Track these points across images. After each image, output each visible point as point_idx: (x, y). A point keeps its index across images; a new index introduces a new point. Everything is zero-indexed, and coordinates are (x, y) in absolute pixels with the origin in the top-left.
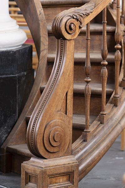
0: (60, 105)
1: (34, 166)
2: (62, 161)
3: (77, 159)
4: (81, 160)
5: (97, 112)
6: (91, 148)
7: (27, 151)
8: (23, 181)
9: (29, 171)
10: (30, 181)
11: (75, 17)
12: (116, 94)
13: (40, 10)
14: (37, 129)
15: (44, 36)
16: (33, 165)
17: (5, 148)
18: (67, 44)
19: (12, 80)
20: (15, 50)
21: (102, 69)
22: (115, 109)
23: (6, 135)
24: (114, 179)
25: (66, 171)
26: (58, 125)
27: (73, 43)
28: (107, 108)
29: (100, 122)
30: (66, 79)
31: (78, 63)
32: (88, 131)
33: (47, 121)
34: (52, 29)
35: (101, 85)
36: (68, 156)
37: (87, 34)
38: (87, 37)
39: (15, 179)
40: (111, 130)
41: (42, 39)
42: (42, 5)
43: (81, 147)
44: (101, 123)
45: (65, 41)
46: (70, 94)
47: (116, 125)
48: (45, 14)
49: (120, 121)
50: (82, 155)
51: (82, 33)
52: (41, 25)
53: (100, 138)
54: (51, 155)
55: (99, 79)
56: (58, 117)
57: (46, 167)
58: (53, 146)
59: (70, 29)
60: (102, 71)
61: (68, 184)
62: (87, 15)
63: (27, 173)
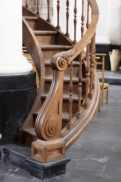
0: (55, 108)
1: (39, 145)
2: (56, 142)
3: (64, 140)
4: (66, 141)
5: (75, 111)
6: (72, 133)
7: (34, 133)
8: (33, 153)
9: (36, 147)
10: (37, 153)
11: (65, 57)
12: (86, 101)
13: (40, 52)
14: (42, 124)
15: (43, 67)
16: (39, 144)
17: (21, 131)
18: (60, 73)
19: (26, 91)
20: (26, 75)
21: (79, 88)
22: (85, 110)
23: (21, 123)
24: (80, 145)
25: (58, 147)
26: (54, 121)
27: (63, 72)
28: (81, 109)
29: (77, 118)
30: (59, 94)
31: (66, 83)
32: (71, 123)
33: (48, 119)
34: (51, 63)
35: (78, 96)
36: (59, 139)
37: (71, 67)
38: (71, 69)
39: (28, 149)
40: (83, 123)
41: (42, 69)
42: (41, 49)
43: (67, 132)
44: (78, 119)
45: (59, 71)
46: (61, 102)
47: (86, 120)
48: (43, 55)
49: (88, 117)
50: (67, 137)
51: (69, 66)
52: (41, 60)
53: (78, 127)
54: (50, 138)
55: (77, 93)
56: (54, 116)
57: (47, 146)
58: (50, 133)
59: (61, 64)
60: (79, 89)
61: (59, 154)
62: (71, 56)
63: (35, 149)
